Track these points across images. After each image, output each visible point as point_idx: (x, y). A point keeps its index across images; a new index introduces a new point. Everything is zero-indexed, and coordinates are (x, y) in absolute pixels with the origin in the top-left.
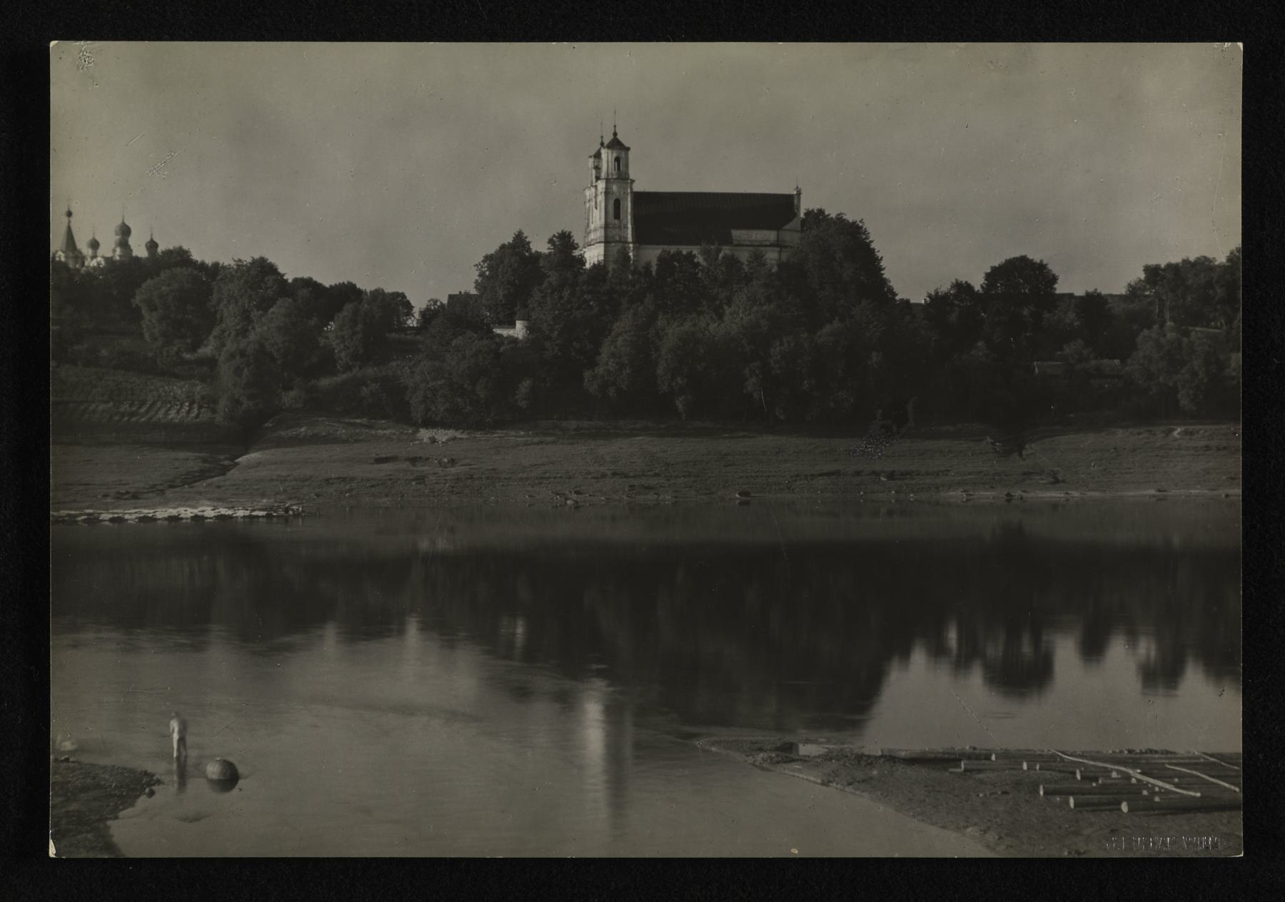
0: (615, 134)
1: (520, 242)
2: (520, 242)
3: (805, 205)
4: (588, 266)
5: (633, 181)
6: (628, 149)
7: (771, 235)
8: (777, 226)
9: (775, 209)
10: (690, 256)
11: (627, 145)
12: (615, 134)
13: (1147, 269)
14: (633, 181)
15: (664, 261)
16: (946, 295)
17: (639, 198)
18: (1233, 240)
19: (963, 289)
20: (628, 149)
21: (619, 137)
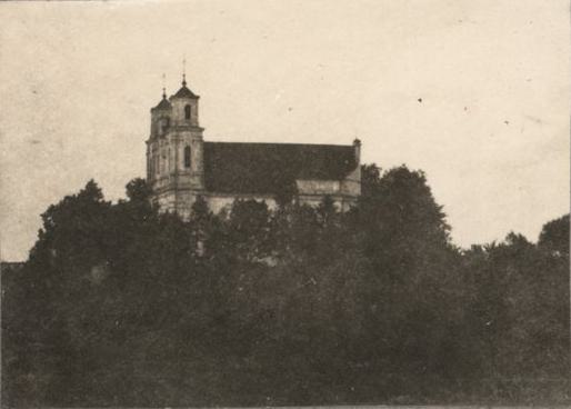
0: (184, 83)
1: (92, 190)
2: (92, 190)
3: (366, 158)
4: (381, 176)
5: (202, 130)
6: (198, 97)
7: (335, 187)
8: (340, 176)
9: (340, 159)
10: (263, 206)
11: (196, 93)
12: (184, 83)
13: (512, 236)
14: (202, 130)
15: (237, 208)
16: (502, 246)
17: (210, 149)
18: (568, 211)
19: (518, 241)
20: (198, 97)
21: (188, 86)
